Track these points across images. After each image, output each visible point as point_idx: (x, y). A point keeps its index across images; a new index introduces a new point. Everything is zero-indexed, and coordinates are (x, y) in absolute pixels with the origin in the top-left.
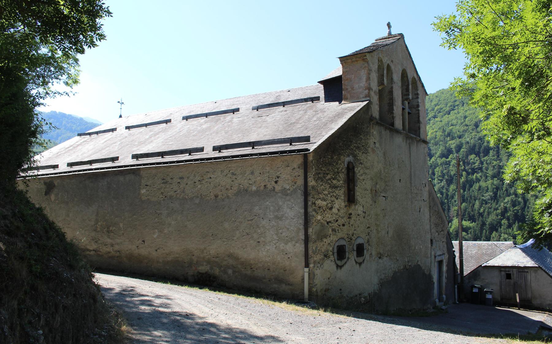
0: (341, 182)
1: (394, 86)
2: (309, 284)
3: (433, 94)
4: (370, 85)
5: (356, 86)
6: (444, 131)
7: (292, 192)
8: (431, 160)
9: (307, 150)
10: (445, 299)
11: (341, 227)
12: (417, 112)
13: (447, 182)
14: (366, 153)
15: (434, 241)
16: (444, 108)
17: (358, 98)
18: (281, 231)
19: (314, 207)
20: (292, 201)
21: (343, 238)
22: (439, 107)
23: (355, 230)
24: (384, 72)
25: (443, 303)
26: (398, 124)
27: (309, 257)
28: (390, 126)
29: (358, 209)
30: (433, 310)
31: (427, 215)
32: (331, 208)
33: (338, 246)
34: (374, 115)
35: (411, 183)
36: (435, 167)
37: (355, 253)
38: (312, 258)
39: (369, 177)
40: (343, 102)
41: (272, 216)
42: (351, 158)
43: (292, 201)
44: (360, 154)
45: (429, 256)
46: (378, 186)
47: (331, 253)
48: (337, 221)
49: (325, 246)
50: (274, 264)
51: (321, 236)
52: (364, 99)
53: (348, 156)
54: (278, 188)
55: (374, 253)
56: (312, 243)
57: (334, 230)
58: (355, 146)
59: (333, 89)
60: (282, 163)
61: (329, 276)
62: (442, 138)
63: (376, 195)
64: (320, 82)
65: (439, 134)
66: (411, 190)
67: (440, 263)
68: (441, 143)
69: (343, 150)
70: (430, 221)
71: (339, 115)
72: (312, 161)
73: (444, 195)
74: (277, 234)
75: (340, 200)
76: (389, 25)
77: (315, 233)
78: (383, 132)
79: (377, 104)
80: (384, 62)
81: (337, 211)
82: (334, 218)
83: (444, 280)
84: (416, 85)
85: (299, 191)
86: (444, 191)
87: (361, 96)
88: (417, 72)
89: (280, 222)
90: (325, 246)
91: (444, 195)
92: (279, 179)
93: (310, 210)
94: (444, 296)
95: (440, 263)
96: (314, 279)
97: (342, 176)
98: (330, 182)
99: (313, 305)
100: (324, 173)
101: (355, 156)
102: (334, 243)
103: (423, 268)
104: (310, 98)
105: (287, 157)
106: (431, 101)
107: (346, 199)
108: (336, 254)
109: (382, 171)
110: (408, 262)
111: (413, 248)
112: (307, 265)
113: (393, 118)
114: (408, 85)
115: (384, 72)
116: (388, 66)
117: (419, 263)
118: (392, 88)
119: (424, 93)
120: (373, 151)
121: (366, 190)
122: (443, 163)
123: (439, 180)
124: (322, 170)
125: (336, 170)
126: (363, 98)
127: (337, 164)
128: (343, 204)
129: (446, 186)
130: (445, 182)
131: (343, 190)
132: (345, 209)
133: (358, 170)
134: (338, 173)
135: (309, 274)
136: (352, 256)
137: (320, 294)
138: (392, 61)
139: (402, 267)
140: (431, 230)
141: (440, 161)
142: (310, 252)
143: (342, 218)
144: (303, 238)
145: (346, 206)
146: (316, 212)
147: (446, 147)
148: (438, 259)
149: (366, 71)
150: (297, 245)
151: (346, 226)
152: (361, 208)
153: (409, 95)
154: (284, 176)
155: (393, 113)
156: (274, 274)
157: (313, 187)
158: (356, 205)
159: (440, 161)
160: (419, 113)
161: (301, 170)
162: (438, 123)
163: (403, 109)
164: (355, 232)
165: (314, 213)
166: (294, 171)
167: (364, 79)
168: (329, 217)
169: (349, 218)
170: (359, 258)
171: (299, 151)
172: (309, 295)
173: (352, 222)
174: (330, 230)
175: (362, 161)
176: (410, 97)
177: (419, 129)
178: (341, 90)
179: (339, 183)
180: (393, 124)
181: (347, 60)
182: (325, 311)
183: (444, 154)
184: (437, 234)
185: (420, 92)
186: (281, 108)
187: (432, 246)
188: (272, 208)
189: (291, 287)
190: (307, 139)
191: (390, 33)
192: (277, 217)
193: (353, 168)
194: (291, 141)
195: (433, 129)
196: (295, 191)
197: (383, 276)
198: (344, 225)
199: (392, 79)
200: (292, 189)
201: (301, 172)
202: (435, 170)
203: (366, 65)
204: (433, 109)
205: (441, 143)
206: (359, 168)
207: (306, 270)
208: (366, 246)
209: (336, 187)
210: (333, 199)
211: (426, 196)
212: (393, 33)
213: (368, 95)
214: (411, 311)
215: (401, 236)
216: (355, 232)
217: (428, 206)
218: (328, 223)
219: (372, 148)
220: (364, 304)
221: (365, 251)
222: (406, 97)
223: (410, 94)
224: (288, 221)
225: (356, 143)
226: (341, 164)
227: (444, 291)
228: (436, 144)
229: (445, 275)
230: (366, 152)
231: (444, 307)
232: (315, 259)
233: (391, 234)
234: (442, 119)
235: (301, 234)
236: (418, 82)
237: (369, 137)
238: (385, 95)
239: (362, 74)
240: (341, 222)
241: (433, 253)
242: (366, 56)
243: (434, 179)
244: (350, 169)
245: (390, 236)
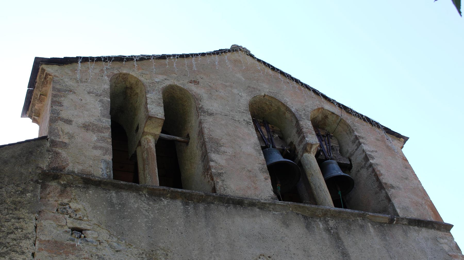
12: (370, 170)
160: (374, 170)
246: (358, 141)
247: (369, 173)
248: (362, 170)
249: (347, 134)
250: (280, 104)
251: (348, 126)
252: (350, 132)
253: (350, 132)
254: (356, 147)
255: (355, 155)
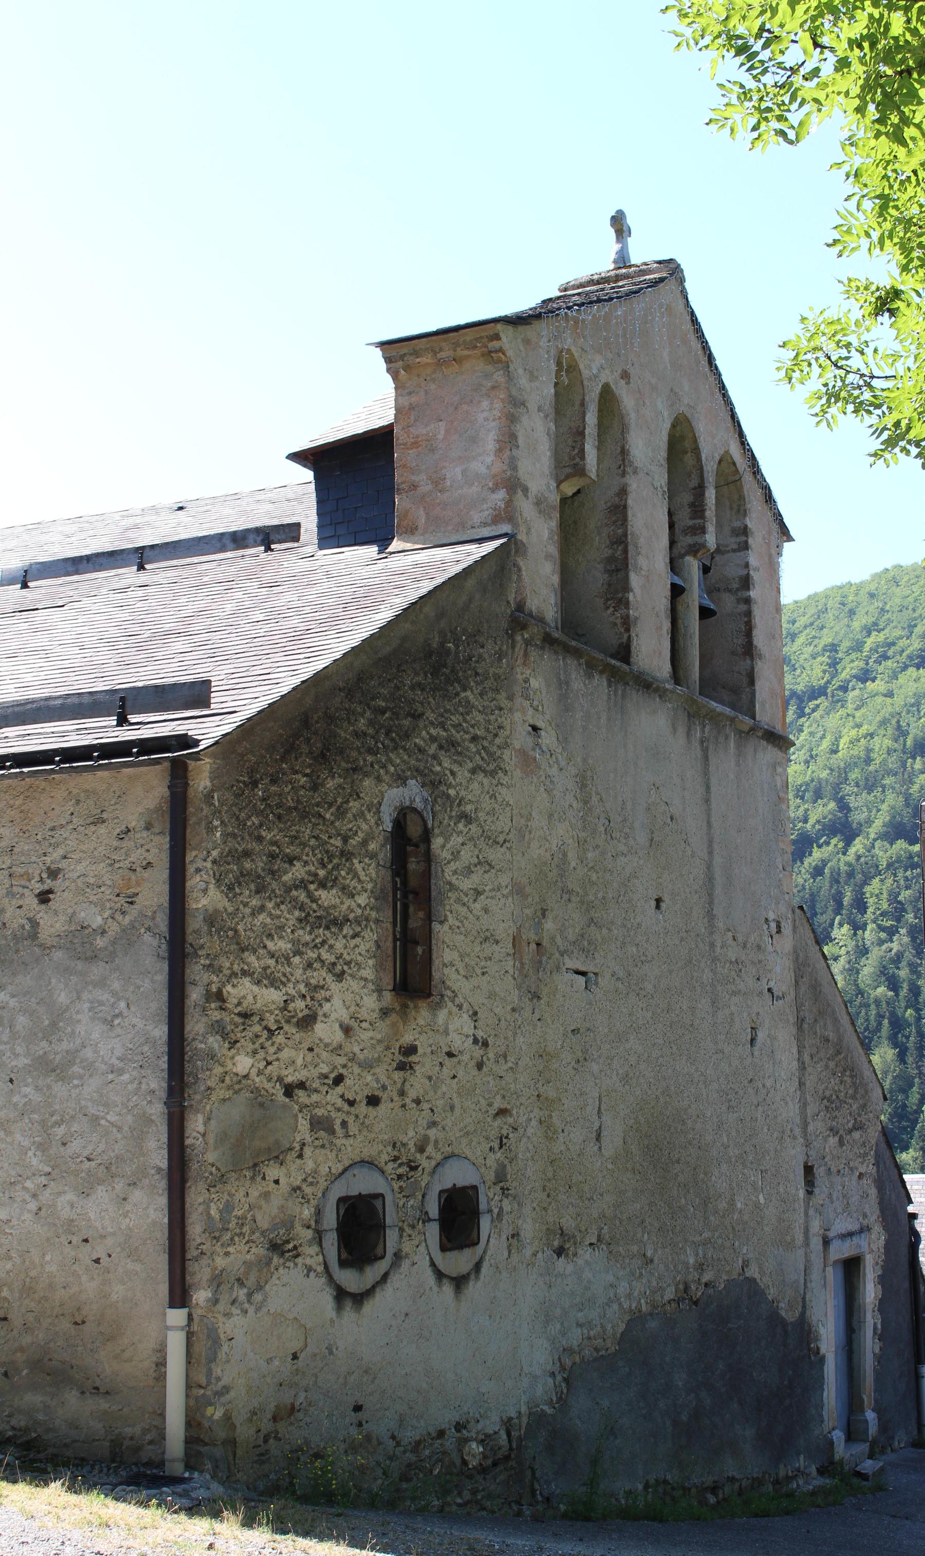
0: (362, 900)
1: (634, 484)
2: (188, 1387)
3: (860, 586)
4: (515, 468)
5: (454, 473)
6: (901, 732)
7: (114, 943)
8: (852, 850)
9: (185, 741)
10: (873, 1429)
11: (362, 1108)
12: (743, 607)
13: (914, 939)
14: (493, 774)
15: (820, 1172)
16: (902, 643)
17: (462, 525)
18: (60, 1131)
19: (216, 1015)
20: (116, 985)
21: (368, 1163)
22: (881, 637)
23: (434, 1124)
24: (586, 418)
25: (862, 1448)
26: (651, 650)
27: (192, 1253)
28: (614, 660)
29: (446, 1027)
30: (819, 1482)
31: (787, 1059)
32: (307, 1022)
33: (341, 1200)
34: (533, 604)
35: (710, 915)
36: (867, 881)
37: (433, 1230)
38: (204, 1261)
39: (504, 879)
40: (396, 545)
41: (23, 1061)
42: (413, 793)
43: (116, 985)
44: (463, 774)
45: (800, 1238)
46: (549, 925)
47: (309, 1234)
48: (339, 1080)
49: (276, 1201)
50: (28, 1290)
51: (255, 1153)
52: (486, 532)
53: (401, 780)
54: (52, 924)
55: (529, 1229)
56: (202, 1186)
57: (317, 1124)
58: (433, 739)
59: (356, 484)
60: (70, 807)
61: (295, 1346)
62: (893, 762)
63: (538, 965)
64: (299, 457)
65: (882, 743)
66: (712, 945)
67: (851, 1268)
68: (887, 781)
69: (371, 751)
70: (801, 1084)
71: (363, 601)
72: (209, 797)
73: (904, 992)
74: (42, 1147)
75: (355, 985)
76: (619, 224)
77: (223, 1137)
78: (578, 682)
79: (548, 557)
80: (586, 373)
81: (339, 1036)
82: (325, 1069)
83: (870, 1345)
84: (740, 490)
85: (147, 937)
86: (904, 973)
87: (476, 517)
88: (741, 434)
89: (60, 1089)
90: (276, 1201)
91: (904, 992)
92: (57, 885)
93: (195, 1026)
94: (870, 1415)
95: (851, 1268)
96: (212, 1359)
97: (369, 874)
98: (302, 896)
99: (201, 1494)
100: (272, 856)
101: (434, 784)
102: (323, 1184)
103: (772, 1293)
104: (257, 530)
105: (97, 779)
106: (852, 613)
107: (388, 981)
108: (331, 1241)
109: (572, 856)
110: (700, 1267)
111: (723, 1205)
112: (179, 1295)
113: (627, 624)
114: (701, 488)
115: (586, 418)
116: (607, 397)
117: (753, 1272)
118: (623, 492)
119: (775, 527)
120: (528, 762)
121: (488, 938)
122: (899, 860)
123: (881, 928)
124: (260, 839)
125: (338, 842)
126: (485, 524)
127: (341, 813)
128: (370, 1003)
129: (909, 955)
130: (906, 939)
131: (370, 937)
132: (383, 1027)
133: (450, 849)
134: (347, 855)
135: (190, 1336)
136: (417, 1247)
137: (245, 1432)
138: (625, 375)
139: (670, 1294)
140: (805, 1125)
141: (884, 853)
142: (195, 1229)
143: (367, 1066)
144: (164, 1164)
145: (385, 1013)
146: (225, 1036)
147: (907, 797)
148: (841, 1250)
149: (498, 405)
150: (137, 1195)
151: (383, 1108)
152: (463, 1022)
153: (703, 530)
154: (80, 868)
155: (627, 604)
156: (27, 1340)
157: (212, 919)
158: (439, 1005)
159: (884, 853)
160: (749, 614)
161: (157, 839)
162: (879, 699)
163: (677, 591)
164: (432, 1133)
165: (214, 1041)
166: (126, 844)
167: (490, 442)
168: (293, 1061)
169: (401, 1067)
170: (452, 1255)
171: (149, 746)
172: (190, 1441)
173: (417, 1085)
174: (303, 1124)
175: (469, 808)
176: (711, 539)
177: (751, 680)
178: (389, 489)
179: (348, 902)
180: (624, 653)
181: (416, 353)
182: (249, 1522)
183: (901, 824)
184: (833, 1141)
185: (756, 520)
186: (129, 575)
187: (810, 1193)
188: (22, 1020)
189: (103, 1404)
190: (196, 695)
191: (622, 260)
192: (47, 1067)
193: (427, 836)
194: (122, 705)
195: (858, 726)
196: (128, 938)
197: (575, 1337)
198: (373, 1101)
199: (624, 452)
200: (113, 929)
201: (157, 848)
202: (868, 889)
203: (499, 377)
204: (858, 646)
205: (887, 781)
206: (456, 840)
207: (177, 1317)
208: (487, 1198)
209: (336, 923)
210: (319, 975)
211: (780, 973)
212: (637, 257)
213: (507, 514)
214: (714, 1490)
215: (663, 1153)
216: (432, 1133)
217: (792, 1019)
218: (289, 1091)
219: (522, 753)
220: (482, 1470)
221: (485, 1223)
222: (689, 540)
223: (711, 528)
224: (94, 1083)
225: (443, 726)
226: (361, 814)
227: (868, 1394)
228: (870, 784)
229: (871, 1320)
230: (491, 768)
231: (868, 1466)
232: (220, 1262)
233: (612, 1143)
234: (894, 686)
235: (152, 1144)
236: (748, 478)
237: (504, 703)
238: (589, 520)
239: (481, 417)
240: (358, 1084)
241: (816, 1226)
242: (497, 337)
243: (864, 927)
244: (409, 843)
245: (608, 1152)
246: (744, 538)
247: (738, 610)
248: (727, 594)
249: (731, 508)
250: (691, 435)
251: (742, 498)
252: (739, 511)
253: (739, 511)
254: (735, 547)
255: (726, 556)
